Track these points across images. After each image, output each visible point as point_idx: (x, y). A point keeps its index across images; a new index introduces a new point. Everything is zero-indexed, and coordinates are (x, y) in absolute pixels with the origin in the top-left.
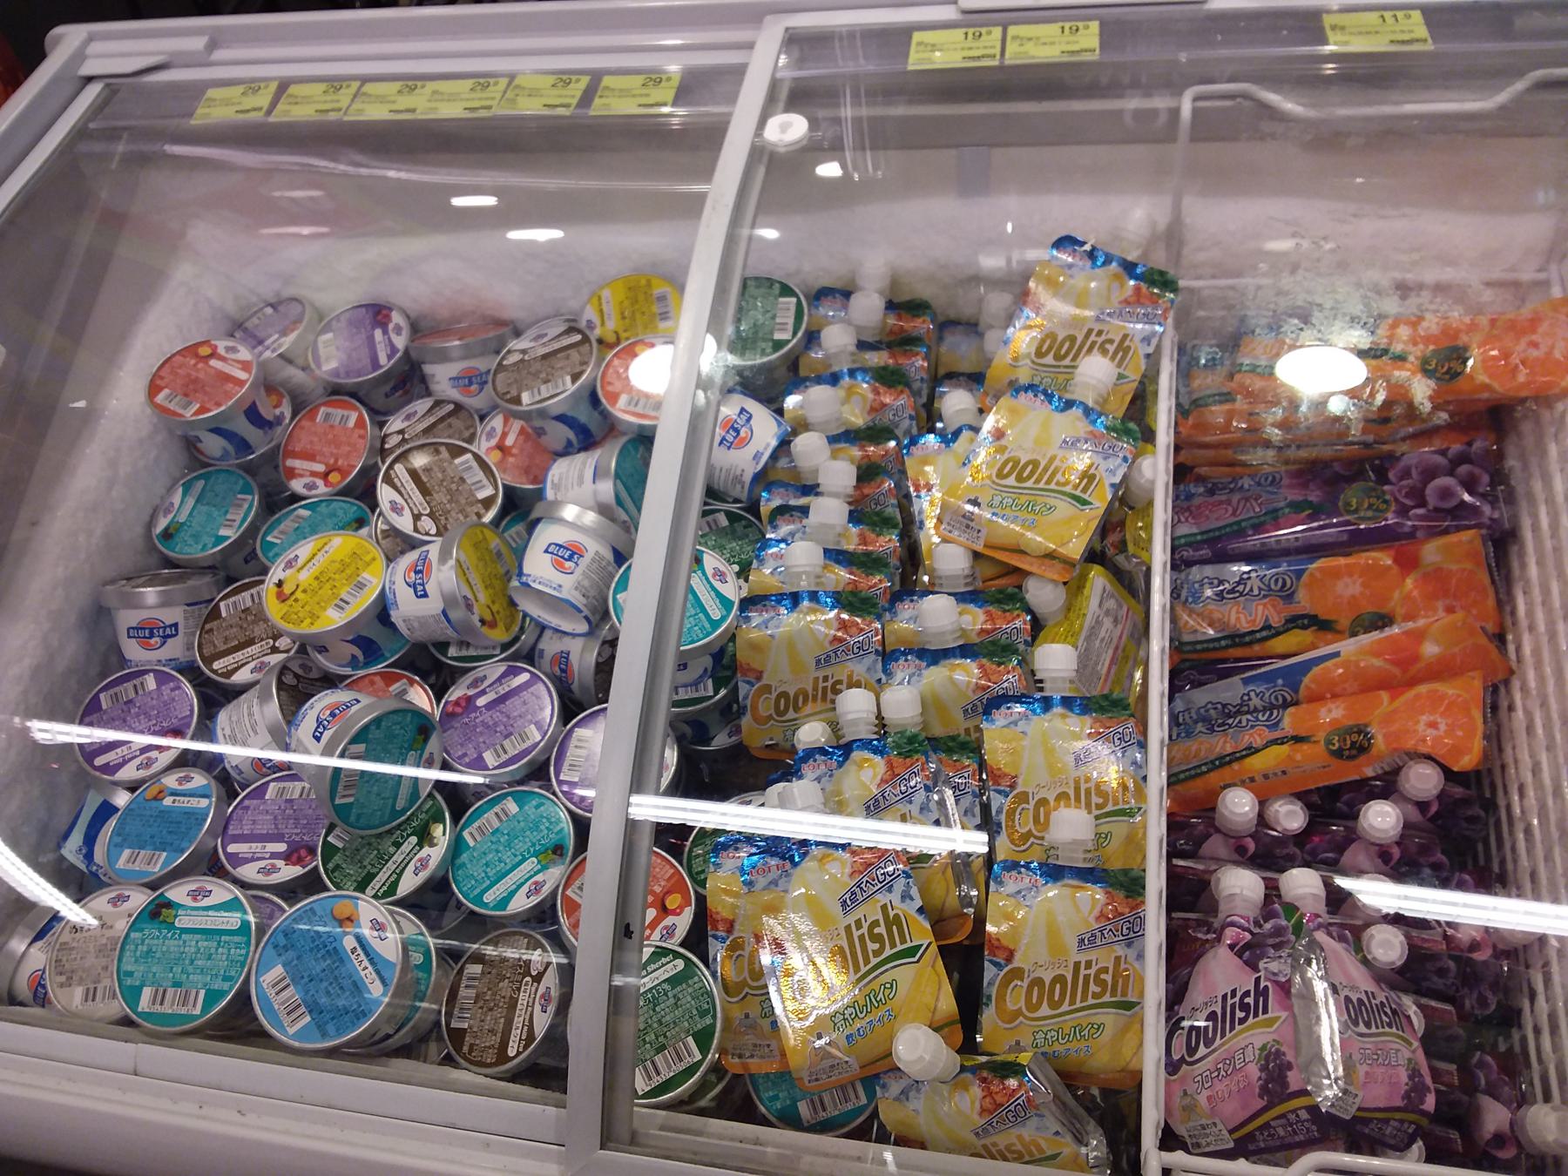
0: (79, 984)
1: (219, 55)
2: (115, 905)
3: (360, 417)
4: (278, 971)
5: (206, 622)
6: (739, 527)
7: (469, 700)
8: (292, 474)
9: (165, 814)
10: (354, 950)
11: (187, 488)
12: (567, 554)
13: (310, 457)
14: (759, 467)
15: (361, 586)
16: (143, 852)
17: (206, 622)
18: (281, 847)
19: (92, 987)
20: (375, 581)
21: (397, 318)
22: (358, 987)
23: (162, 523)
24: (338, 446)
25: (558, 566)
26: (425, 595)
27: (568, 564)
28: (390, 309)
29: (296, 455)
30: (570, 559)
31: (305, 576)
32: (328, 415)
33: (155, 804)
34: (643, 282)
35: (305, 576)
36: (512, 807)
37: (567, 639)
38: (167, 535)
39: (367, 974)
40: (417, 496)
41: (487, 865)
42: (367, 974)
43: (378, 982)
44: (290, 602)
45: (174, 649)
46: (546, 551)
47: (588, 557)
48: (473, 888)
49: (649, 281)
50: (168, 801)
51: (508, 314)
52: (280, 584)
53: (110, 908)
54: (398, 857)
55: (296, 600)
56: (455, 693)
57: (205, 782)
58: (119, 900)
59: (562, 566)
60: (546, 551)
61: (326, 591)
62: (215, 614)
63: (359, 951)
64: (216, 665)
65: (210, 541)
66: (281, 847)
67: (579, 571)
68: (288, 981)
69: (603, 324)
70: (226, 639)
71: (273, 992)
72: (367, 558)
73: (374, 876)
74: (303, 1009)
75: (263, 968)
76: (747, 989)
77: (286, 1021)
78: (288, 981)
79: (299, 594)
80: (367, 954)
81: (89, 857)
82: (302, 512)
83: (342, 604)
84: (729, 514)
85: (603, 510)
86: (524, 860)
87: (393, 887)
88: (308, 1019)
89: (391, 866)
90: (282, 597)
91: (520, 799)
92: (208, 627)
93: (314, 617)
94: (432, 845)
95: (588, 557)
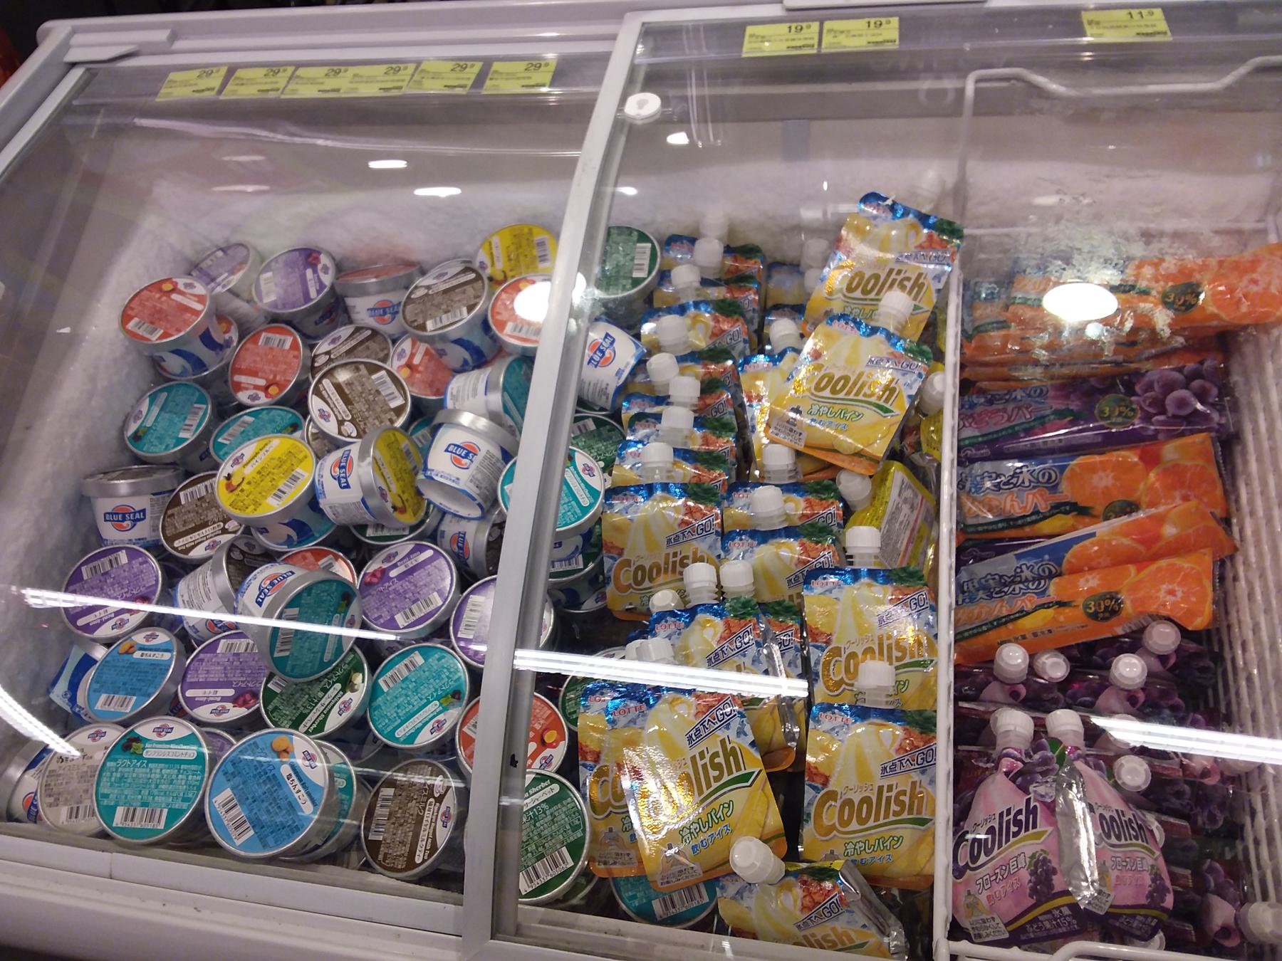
0: (65, 804)
1: (179, 45)
2: (94, 740)
3: (295, 341)
4: (227, 793)
5: (168, 508)
6: (604, 430)
7: (384, 572)
8: (239, 387)
9: (135, 665)
10: (289, 776)
11: (153, 399)
12: (463, 453)
13: (254, 373)
14: (621, 382)
15: (295, 479)
16: (117, 696)
17: (168, 508)
18: (230, 692)
19: (75, 806)
20: (306, 475)
21: (324, 260)
22: (292, 807)
23: (133, 428)
24: (276, 365)
25: (457, 463)
26: (348, 486)
27: (464, 461)
28: (319, 253)
29: (242, 372)
30: (466, 457)
31: (249, 471)
32: (268, 339)
33: (126, 657)
34: (526, 230)
35: (249, 471)
36: (419, 659)
37: (463, 522)
38: (137, 437)
39: (300, 796)
40: (341, 405)
41: (398, 707)
42: (300, 796)
43: (309, 803)
44: (237, 492)
45: (142, 530)
46: (447, 450)
47: (481, 455)
48: (387, 726)
49: (530, 230)
50: (137, 655)
51: (415, 257)
52: (229, 477)
53: (90, 742)
54: (326, 701)
55: (242, 490)
56: (372, 567)
57: (167, 639)
58: (97, 735)
59: (459, 462)
60: (447, 450)
61: (267, 483)
62: (175, 502)
63: (294, 777)
64: (177, 544)
65: (171, 442)
66: (230, 692)
67: (473, 466)
68: (235, 801)
69: (493, 265)
70: (185, 523)
71: (223, 811)
72: (300, 456)
73: (306, 715)
74: (248, 824)
75: (215, 791)
76: (611, 809)
77: (234, 834)
78: (235, 801)
79: (244, 486)
80: (300, 780)
81: (73, 700)
82: (247, 418)
83: (280, 494)
84: (596, 420)
85: (493, 416)
86: (429, 703)
87: (322, 725)
88: (252, 832)
89: (320, 708)
90: (230, 488)
91: (425, 653)
92: (170, 512)
93: (257, 504)
94: (353, 691)
95: (481, 455)
